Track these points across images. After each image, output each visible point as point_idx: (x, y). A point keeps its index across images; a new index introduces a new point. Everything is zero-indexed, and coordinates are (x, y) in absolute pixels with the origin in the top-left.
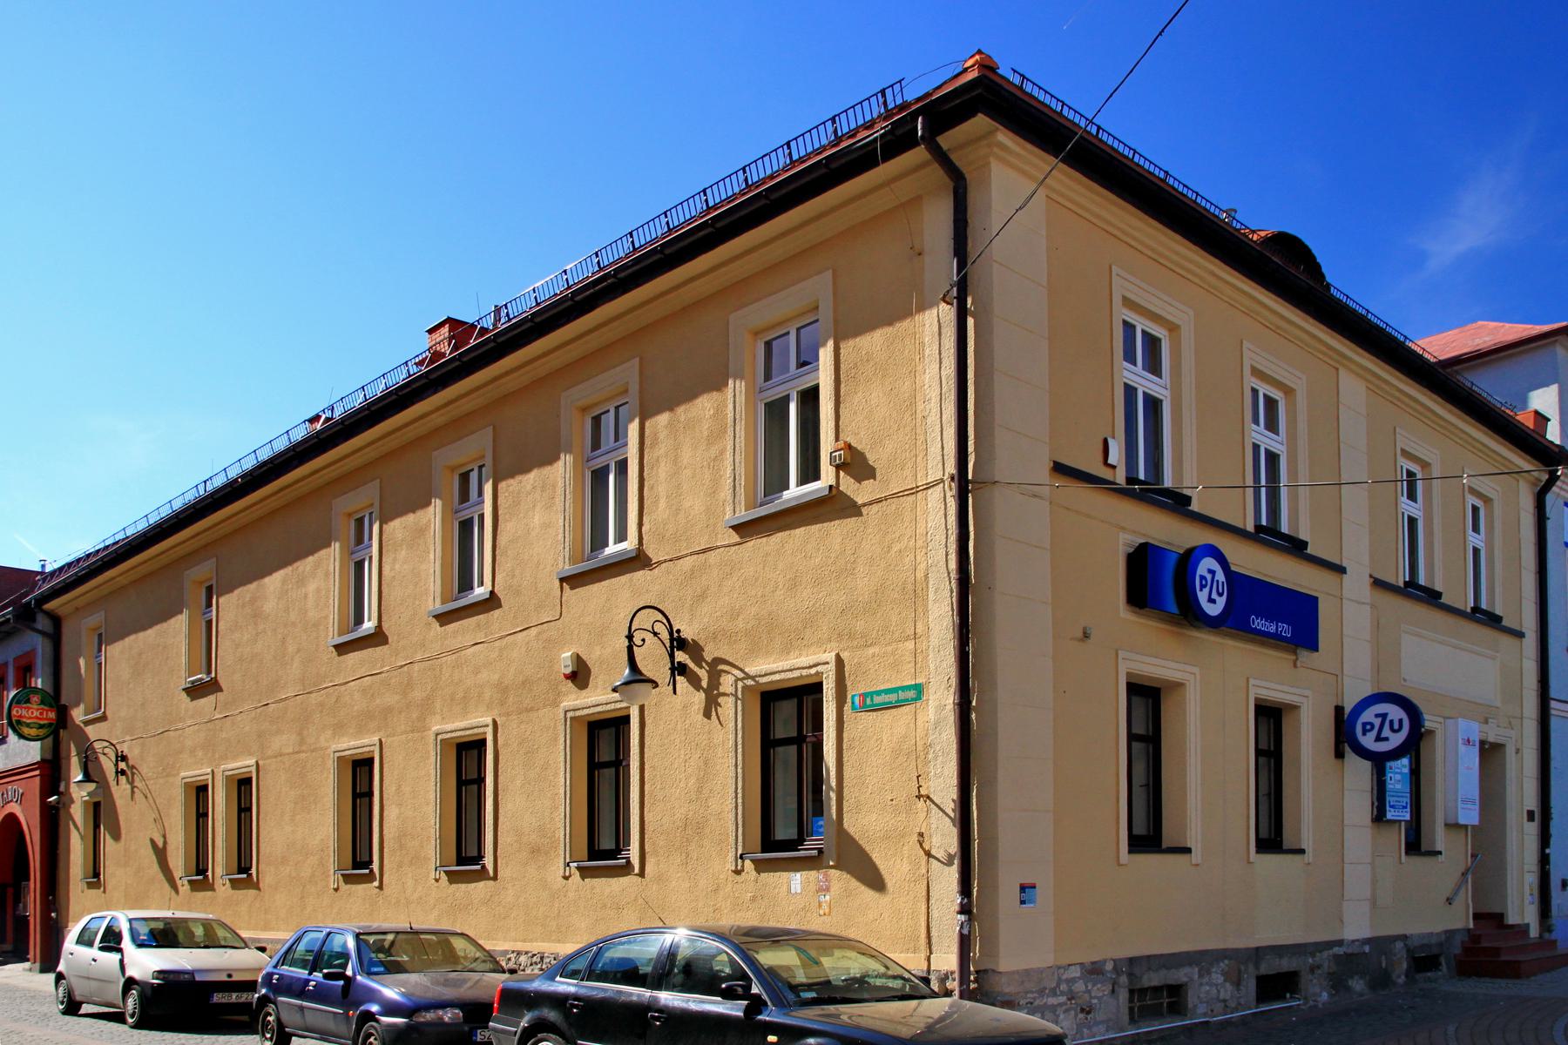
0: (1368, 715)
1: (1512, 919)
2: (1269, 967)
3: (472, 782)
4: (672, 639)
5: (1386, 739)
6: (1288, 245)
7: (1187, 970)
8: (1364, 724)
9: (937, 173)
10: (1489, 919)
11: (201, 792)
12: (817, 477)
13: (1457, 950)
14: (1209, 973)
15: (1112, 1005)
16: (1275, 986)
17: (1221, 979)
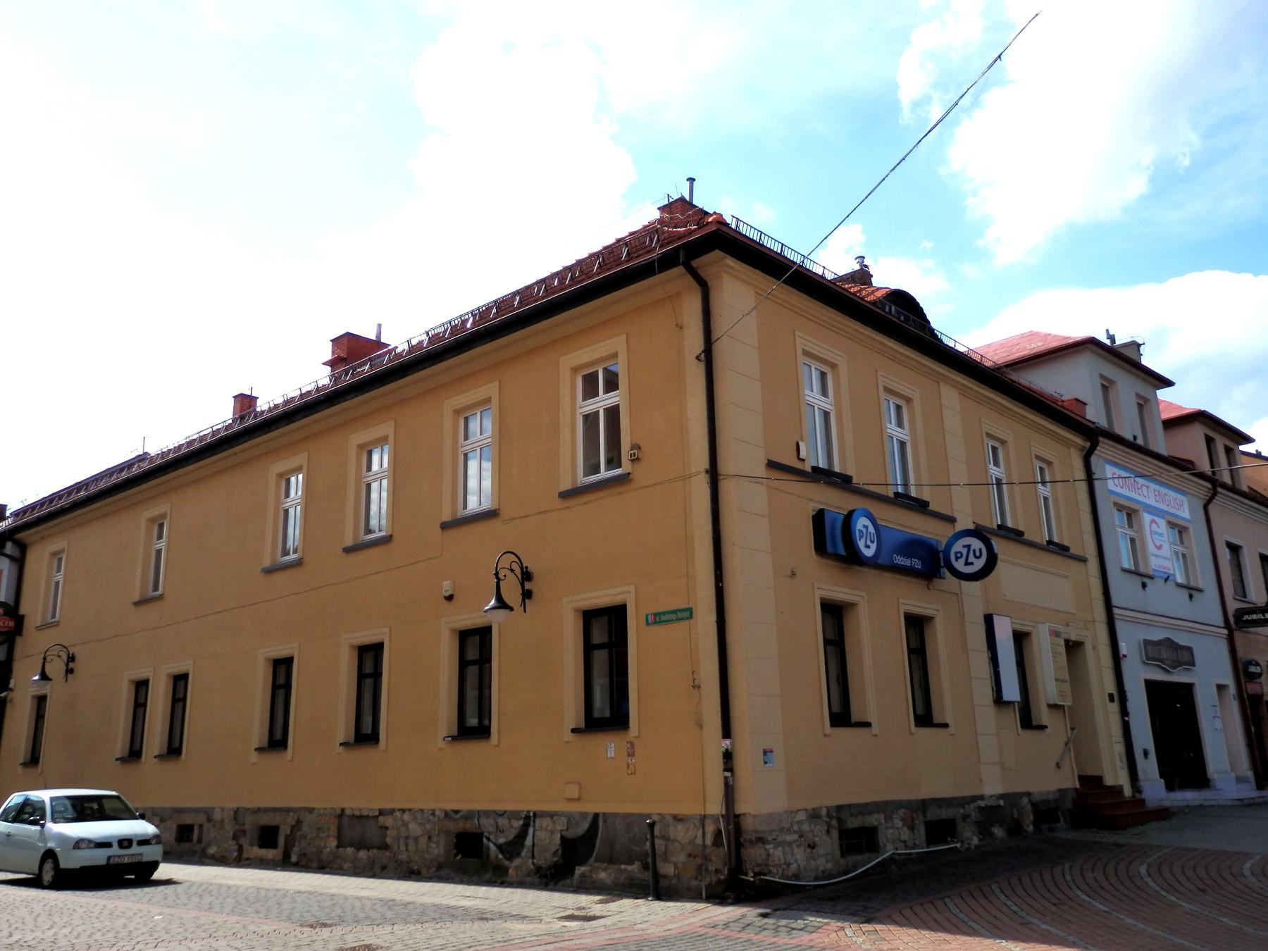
0: (958, 546)
1: (1109, 781)
2: (934, 814)
4: (522, 573)
6: (902, 300)
7: (876, 816)
8: (956, 553)
9: (689, 279)
10: (1091, 782)
11: (141, 686)
12: (619, 466)
13: (1069, 805)
14: (892, 819)
15: (829, 844)
16: (940, 830)
17: (900, 824)
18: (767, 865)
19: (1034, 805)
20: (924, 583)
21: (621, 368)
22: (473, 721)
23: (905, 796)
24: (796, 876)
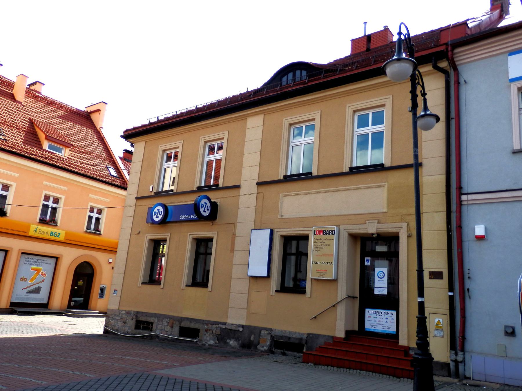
2: (185, 324)
3: (202, 254)
7: (154, 318)
14: (162, 321)
15: (131, 323)
19: (272, 337)
20: (211, 223)
21: (225, 142)
23: (172, 314)
24: (117, 330)
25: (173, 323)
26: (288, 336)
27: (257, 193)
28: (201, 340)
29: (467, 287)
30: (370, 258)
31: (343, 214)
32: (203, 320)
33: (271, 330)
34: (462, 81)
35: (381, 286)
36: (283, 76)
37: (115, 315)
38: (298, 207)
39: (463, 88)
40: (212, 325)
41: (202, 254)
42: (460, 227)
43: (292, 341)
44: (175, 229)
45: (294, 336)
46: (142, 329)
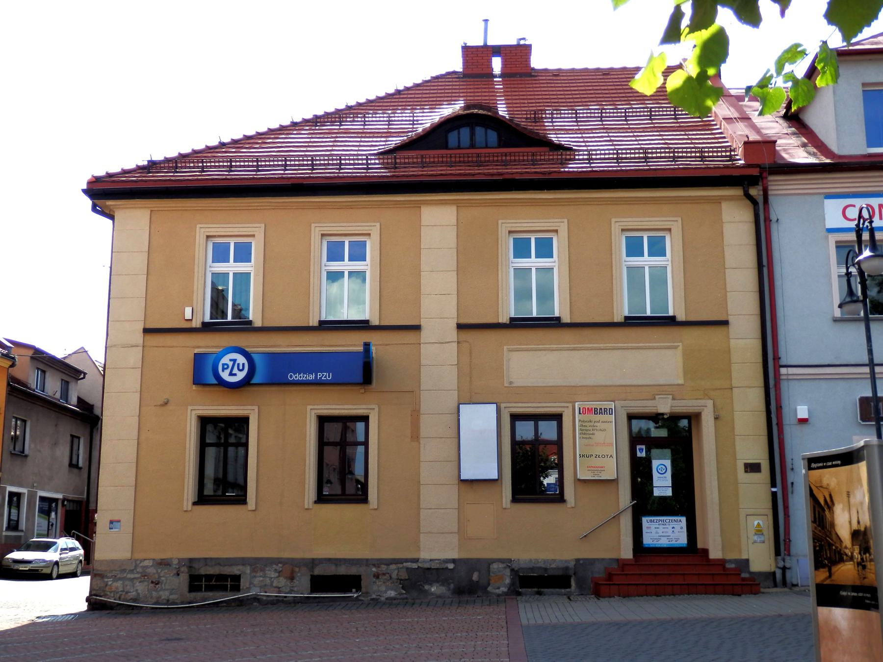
0: (226, 360)
5: (235, 375)
7: (240, 567)
8: (223, 365)
14: (263, 570)
18: (104, 591)
22: (15, 499)
23: (286, 555)
24: (135, 600)
25: (293, 572)
26: (543, 566)
27: (458, 343)
28: (367, 593)
29: (789, 481)
30: (644, 447)
31: (618, 384)
32: (367, 560)
33: (510, 561)
34: (773, 217)
35: (662, 484)
36: (452, 130)
37: (124, 571)
38: (534, 368)
39: (774, 227)
40: (388, 565)
41: (232, 445)
42: (779, 408)
43: (551, 573)
44: (274, 398)
45: (553, 566)
46: (205, 591)
